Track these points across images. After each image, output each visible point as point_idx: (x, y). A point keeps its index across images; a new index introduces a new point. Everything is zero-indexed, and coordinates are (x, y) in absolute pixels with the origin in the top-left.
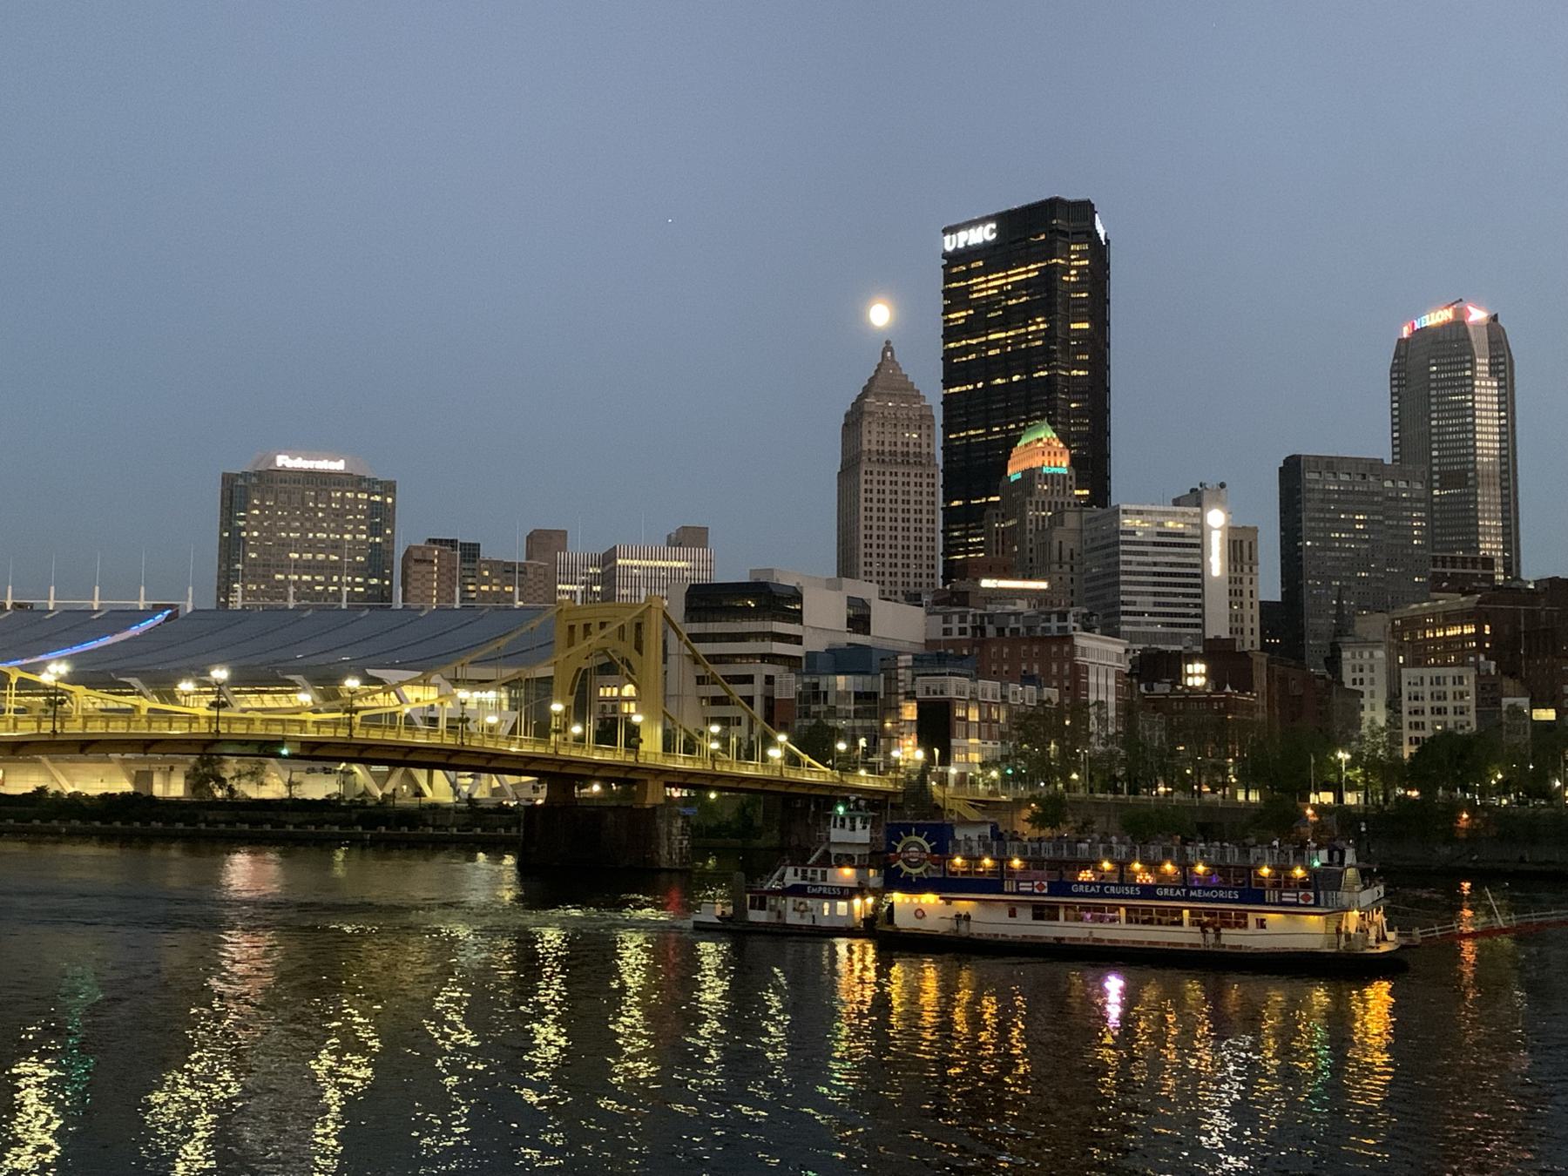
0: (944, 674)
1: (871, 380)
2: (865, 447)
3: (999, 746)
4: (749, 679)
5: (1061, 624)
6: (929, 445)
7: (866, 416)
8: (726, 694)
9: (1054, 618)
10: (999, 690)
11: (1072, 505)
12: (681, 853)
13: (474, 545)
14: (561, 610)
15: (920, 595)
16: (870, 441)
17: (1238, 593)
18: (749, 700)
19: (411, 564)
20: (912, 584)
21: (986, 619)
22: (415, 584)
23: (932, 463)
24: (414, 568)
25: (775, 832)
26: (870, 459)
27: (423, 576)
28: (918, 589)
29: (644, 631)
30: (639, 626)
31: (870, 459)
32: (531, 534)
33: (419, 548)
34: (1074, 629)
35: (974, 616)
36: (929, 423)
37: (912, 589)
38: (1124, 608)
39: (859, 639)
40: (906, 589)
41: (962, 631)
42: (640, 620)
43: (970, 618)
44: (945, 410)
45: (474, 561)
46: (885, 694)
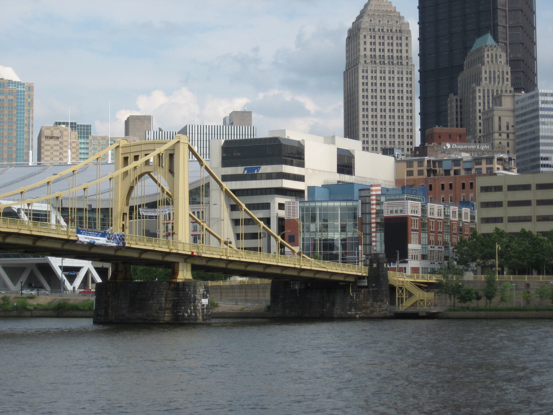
0: (403, 199)
1: (366, 6)
2: (362, 53)
3: (443, 249)
4: (267, 206)
5: (489, 166)
6: (407, 51)
7: (361, 30)
8: (235, 204)
9: (484, 162)
10: (443, 211)
11: (508, 92)
12: (203, 312)
13: (87, 126)
14: (118, 147)
15: (393, 149)
16: (365, 49)
17: (517, 79)
18: (267, 221)
19: (43, 139)
20: (388, 143)
21: (437, 164)
22: (46, 153)
23: (409, 64)
24: (45, 142)
25: (280, 306)
26: (365, 61)
27: (52, 148)
28: (392, 146)
29: (175, 160)
30: (171, 156)
31: (365, 61)
32: (128, 118)
33: (48, 128)
34: (498, 169)
35: (429, 161)
36: (406, 35)
37: (388, 146)
38: (542, 162)
39: (346, 178)
40: (383, 146)
41: (420, 173)
42: (171, 152)
43: (426, 163)
44: (421, 29)
45: (87, 138)
46: (362, 214)
